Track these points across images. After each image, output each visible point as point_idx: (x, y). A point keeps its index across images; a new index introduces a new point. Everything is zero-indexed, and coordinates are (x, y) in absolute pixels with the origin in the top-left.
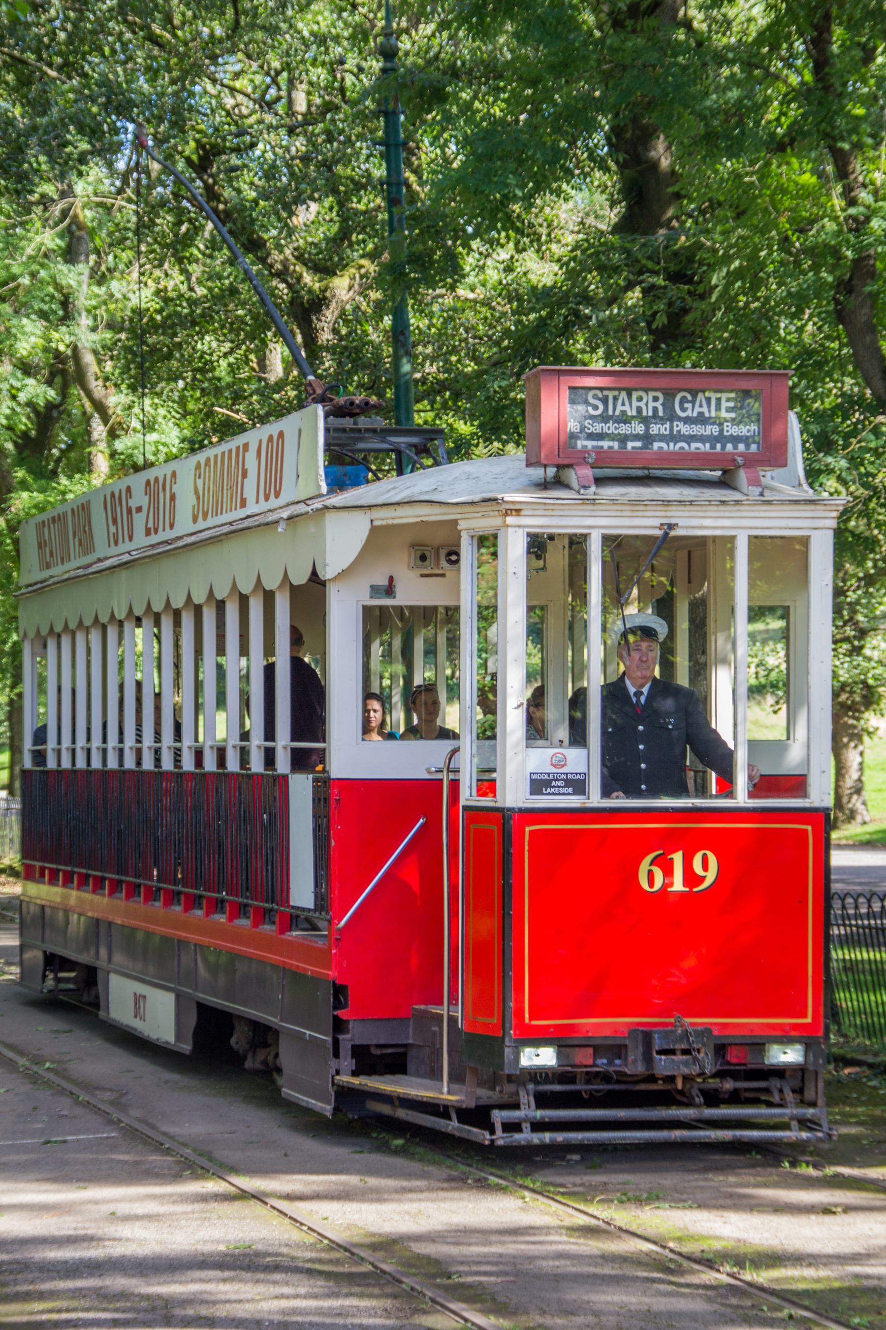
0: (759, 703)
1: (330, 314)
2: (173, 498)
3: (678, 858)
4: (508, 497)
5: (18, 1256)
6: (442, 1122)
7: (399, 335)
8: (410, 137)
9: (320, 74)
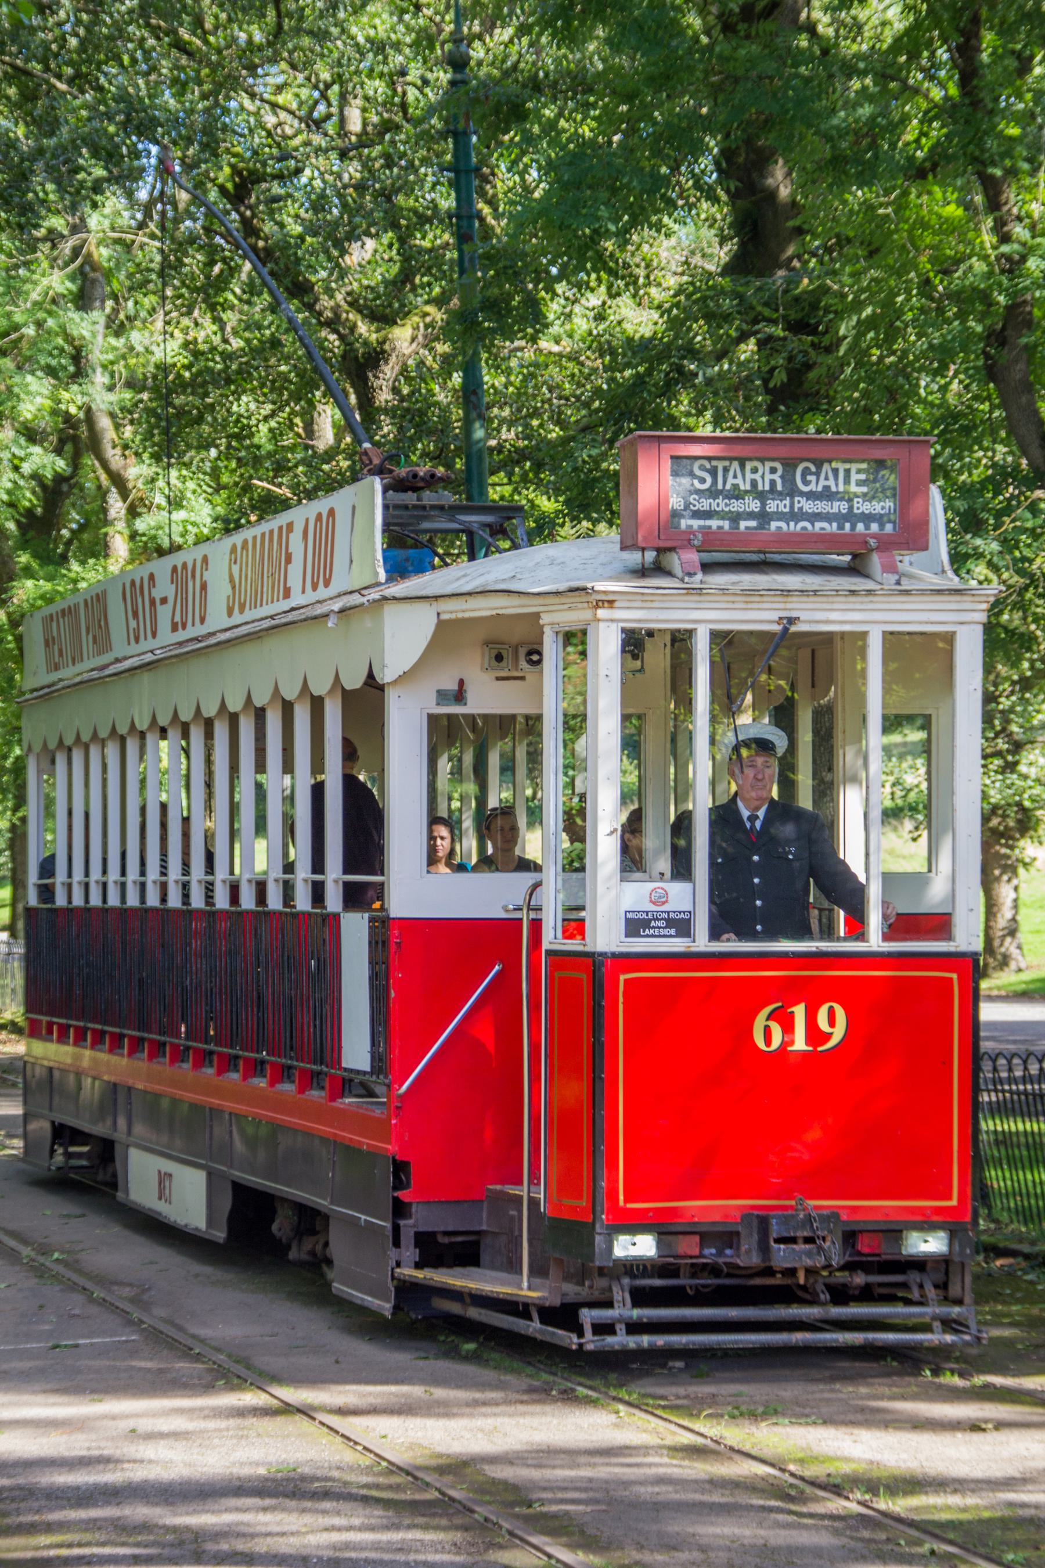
0: (895, 829)
1: (389, 370)
2: (204, 587)
3: (799, 1011)
4: (600, 586)
5: (21, 1481)
6: (522, 1322)
8: (484, 161)
9: (377, 87)
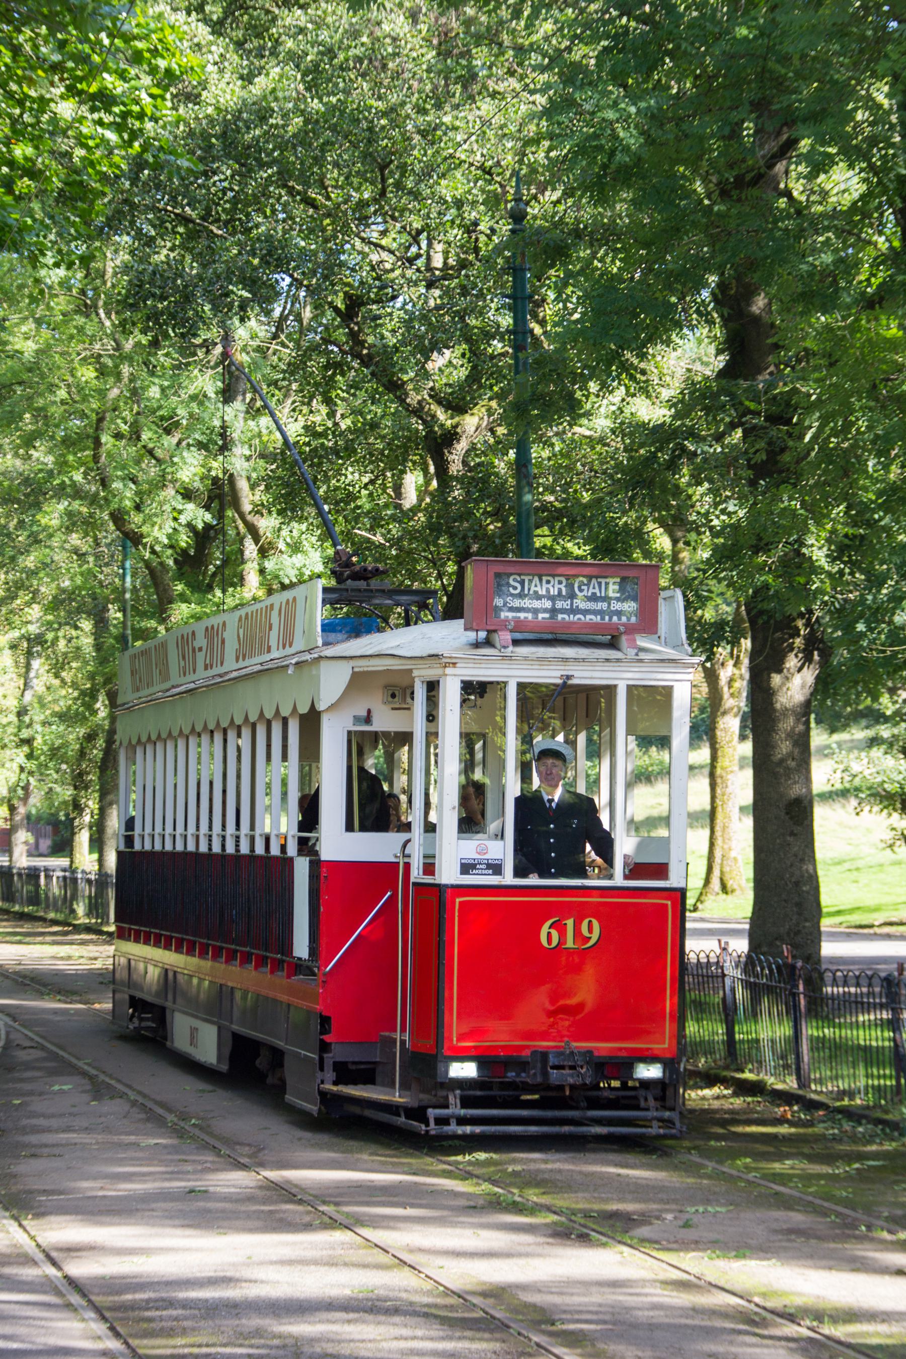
0: (844, 806)
1: (461, 446)
2: (223, 642)
3: (570, 923)
5: (164, 1295)
6: (395, 1118)
8: (536, 291)
9: (456, 234)
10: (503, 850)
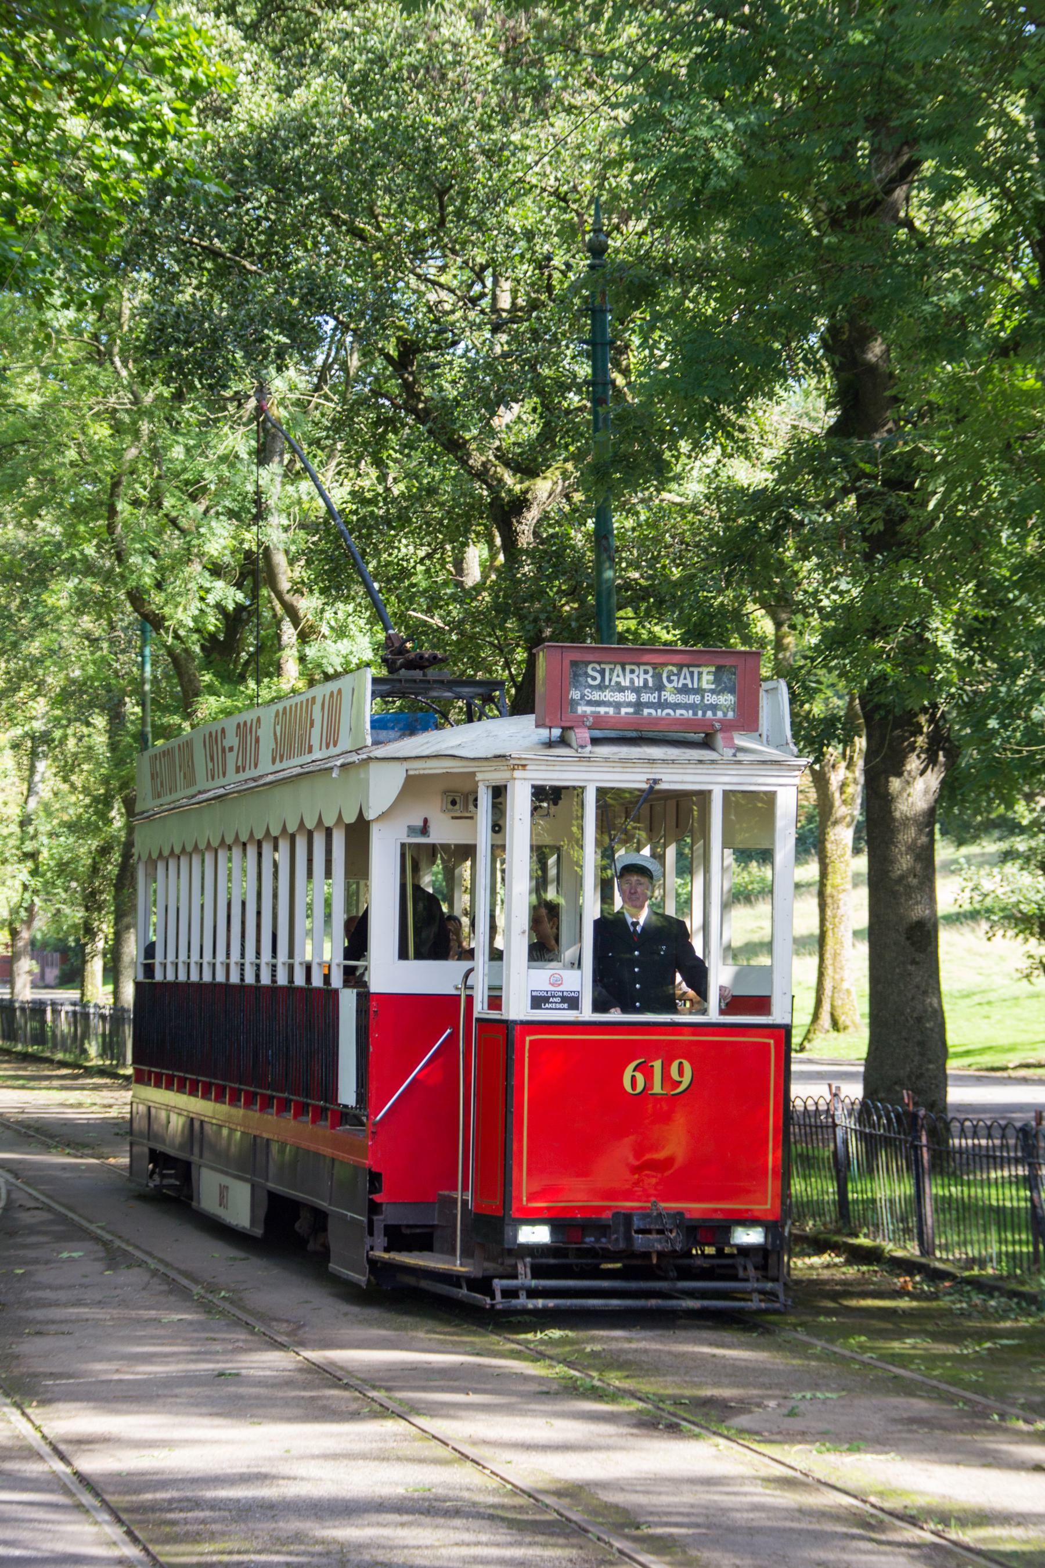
0: (973, 930)
1: (532, 515)
2: (257, 740)
3: (657, 1065)
5: (189, 1494)
6: (455, 1290)
7: (602, 536)
8: (618, 336)
9: (525, 270)
10: (580, 981)
